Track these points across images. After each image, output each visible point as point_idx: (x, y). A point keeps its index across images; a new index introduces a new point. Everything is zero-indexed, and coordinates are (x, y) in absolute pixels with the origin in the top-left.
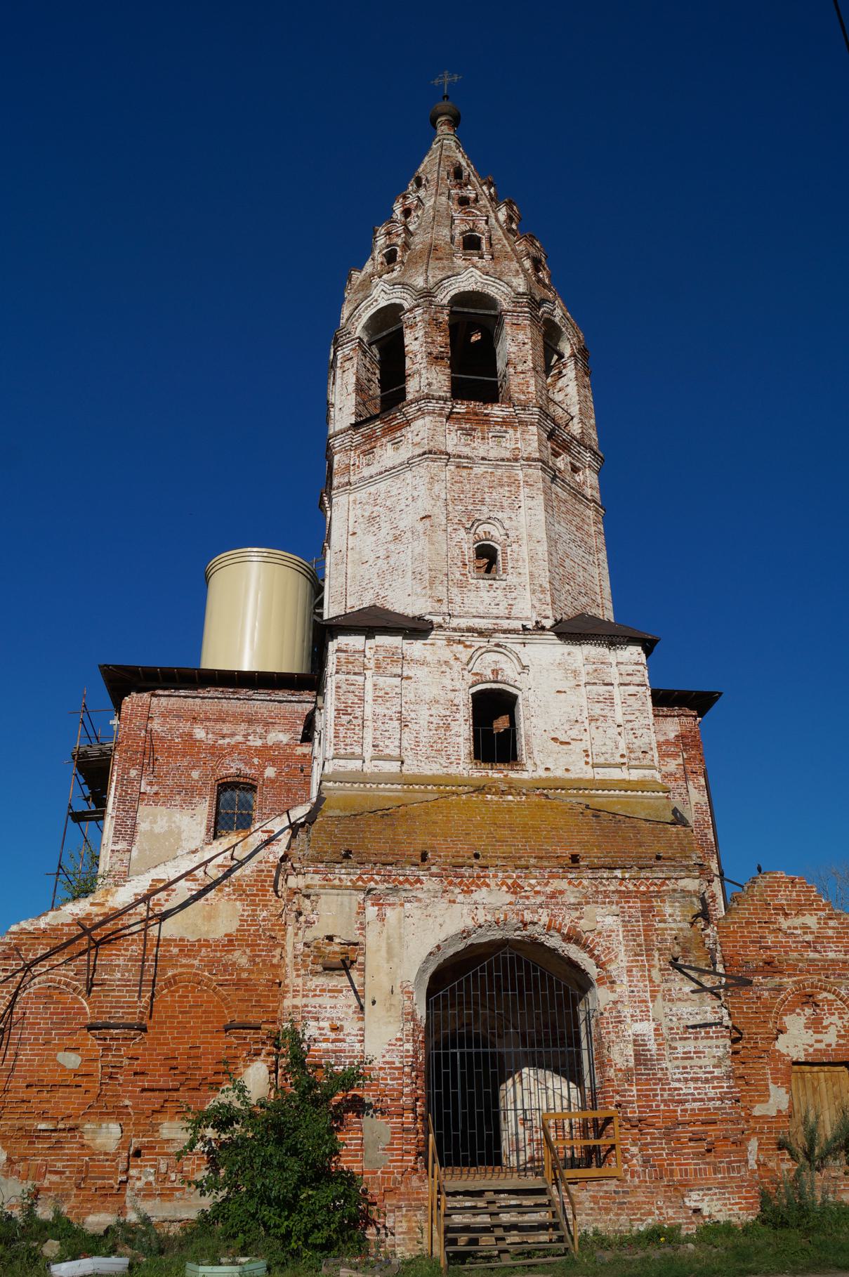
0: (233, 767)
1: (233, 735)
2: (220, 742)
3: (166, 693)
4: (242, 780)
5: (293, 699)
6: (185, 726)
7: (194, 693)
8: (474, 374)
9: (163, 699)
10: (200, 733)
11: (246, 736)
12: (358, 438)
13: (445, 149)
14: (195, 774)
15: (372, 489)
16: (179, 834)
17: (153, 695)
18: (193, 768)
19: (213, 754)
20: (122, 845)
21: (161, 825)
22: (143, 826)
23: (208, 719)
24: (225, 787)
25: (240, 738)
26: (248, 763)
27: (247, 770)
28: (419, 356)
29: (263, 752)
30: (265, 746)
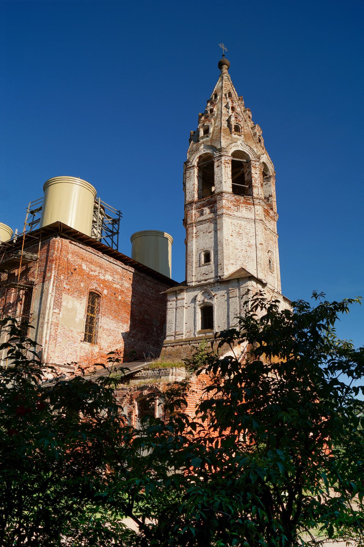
0: (94, 286)
1: (95, 271)
2: (91, 273)
3: (75, 243)
4: (97, 292)
5: (115, 263)
6: (79, 261)
7: (85, 247)
8: (242, 186)
9: (73, 245)
10: (84, 267)
11: (99, 273)
12: (233, 199)
13: (226, 84)
14: (82, 285)
15: (239, 222)
16: (76, 310)
17: (70, 243)
18: (82, 281)
19: (88, 278)
20: (57, 311)
21: (70, 305)
22: (64, 304)
23: (87, 261)
24: (91, 293)
25: (97, 273)
26: (99, 285)
27: (99, 289)
28: (257, 181)
29: (104, 281)
30: (104, 280)
